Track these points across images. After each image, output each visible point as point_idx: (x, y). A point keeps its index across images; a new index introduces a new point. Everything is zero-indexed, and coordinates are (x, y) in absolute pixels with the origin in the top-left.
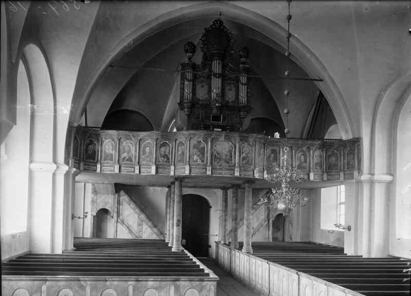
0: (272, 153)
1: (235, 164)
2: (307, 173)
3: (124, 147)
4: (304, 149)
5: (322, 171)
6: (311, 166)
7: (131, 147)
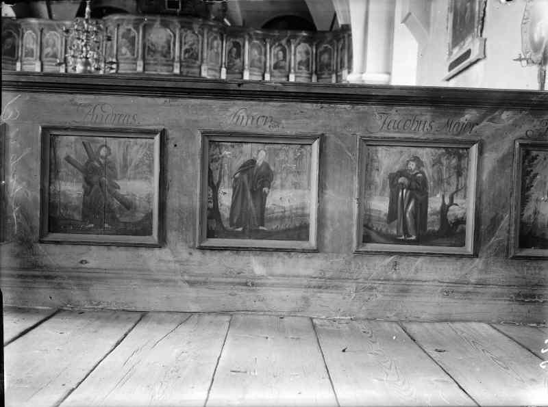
0: (234, 46)
1: (174, 58)
2: (287, 74)
3: (48, 40)
4: (284, 42)
5: (310, 72)
6: (292, 65)
7: (56, 39)
